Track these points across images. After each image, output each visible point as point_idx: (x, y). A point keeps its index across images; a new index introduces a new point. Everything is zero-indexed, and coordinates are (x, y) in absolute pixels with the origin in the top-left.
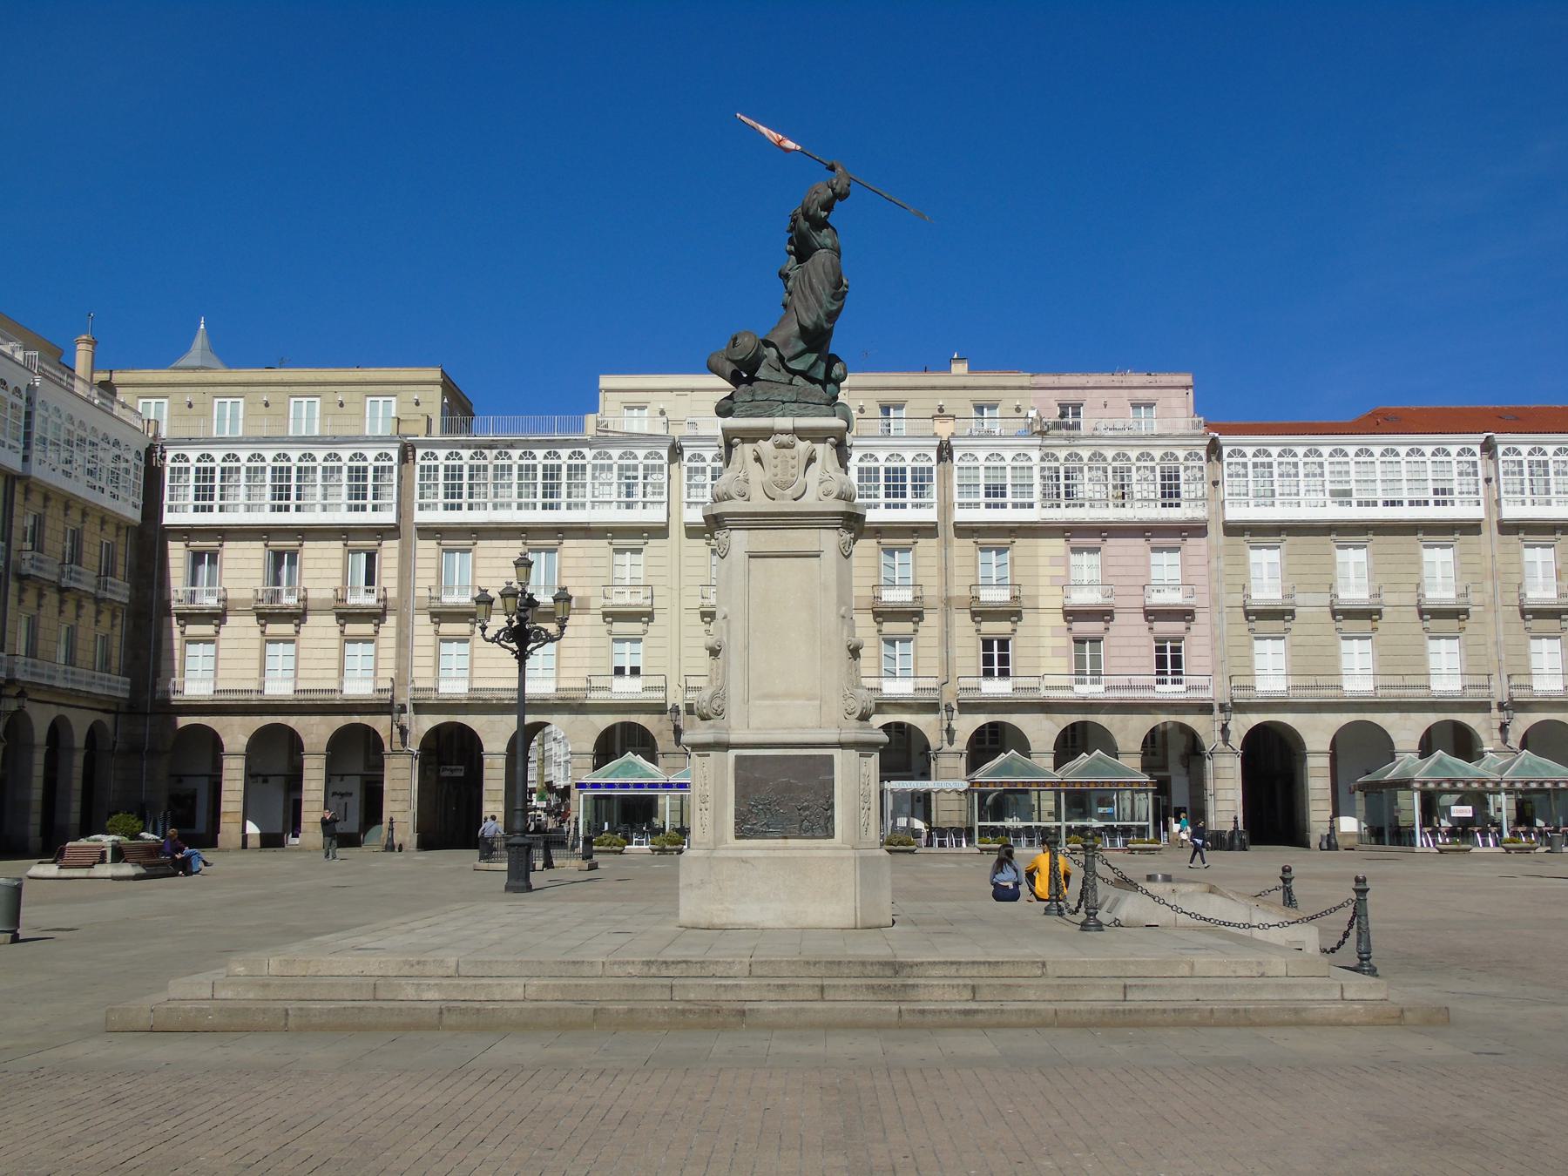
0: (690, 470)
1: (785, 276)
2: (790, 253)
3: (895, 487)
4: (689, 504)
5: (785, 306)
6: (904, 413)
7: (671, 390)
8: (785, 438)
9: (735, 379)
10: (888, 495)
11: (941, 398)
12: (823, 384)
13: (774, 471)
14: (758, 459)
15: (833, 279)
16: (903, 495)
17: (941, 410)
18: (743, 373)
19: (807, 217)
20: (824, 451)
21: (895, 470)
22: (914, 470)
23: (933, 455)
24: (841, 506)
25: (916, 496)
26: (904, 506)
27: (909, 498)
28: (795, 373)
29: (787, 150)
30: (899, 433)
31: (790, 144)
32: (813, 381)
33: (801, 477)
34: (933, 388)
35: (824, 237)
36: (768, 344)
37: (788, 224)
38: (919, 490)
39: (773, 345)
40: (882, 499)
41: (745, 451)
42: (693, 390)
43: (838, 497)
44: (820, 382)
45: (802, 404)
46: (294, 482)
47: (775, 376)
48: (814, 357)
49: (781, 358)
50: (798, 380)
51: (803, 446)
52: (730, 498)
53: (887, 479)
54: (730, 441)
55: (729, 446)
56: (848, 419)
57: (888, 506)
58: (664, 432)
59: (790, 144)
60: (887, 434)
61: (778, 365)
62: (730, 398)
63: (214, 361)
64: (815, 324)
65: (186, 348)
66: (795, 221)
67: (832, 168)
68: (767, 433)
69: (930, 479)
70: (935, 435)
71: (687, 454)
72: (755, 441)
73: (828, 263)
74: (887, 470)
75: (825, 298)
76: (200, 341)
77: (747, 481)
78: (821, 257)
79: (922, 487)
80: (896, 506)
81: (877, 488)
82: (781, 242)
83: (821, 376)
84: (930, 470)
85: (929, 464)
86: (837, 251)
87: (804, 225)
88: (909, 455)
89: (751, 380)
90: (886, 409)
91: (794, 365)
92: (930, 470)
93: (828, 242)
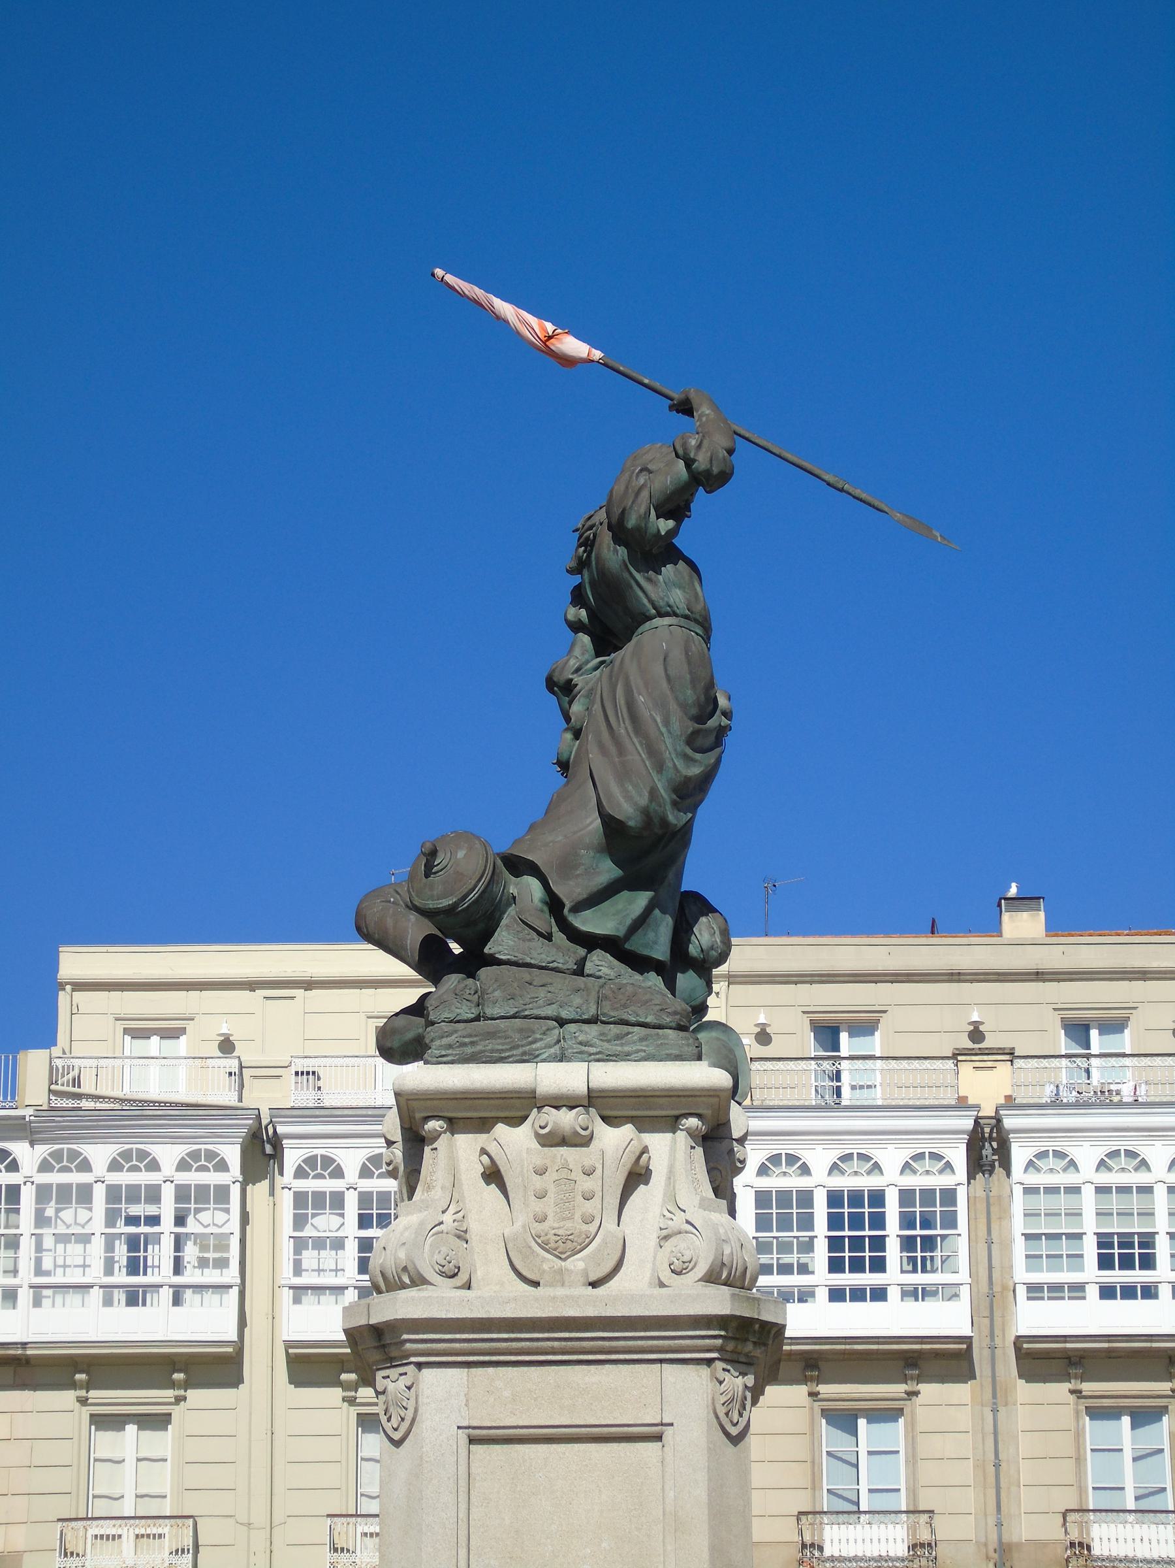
0: (300, 1199)
1: (563, 689)
2: (576, 627)
3: (857, 1243)
4: (299, 1292)
5: (564, 766)
6: (875, 1044)
7: (251, 985)
8: (566, 1119)
9: (431, 961)
10: (835, 1266)
11: (978, 1004)
12: (667, 971)
13: (537, 1206)
14: (493, 1176)
15: (690, 695)
16: (879, 1265)
17: (976, 1034)
18: (453, 944)
19: (619, 531)
20: (672, 1152)
21: (856, 1198)
22: (906, 1196)
23: (958, 1155)
24: (719, 1302)
25: (913, 1265)
26: (879, 1294)
27: (894, 1275)
28: (590, 942)
29: (568, 361)
30: (863, 1097)
31: (573, 346)
32: (639, 963)
33: (610, 1224)
34: (955, 977)
35: (667, 586)
36: (517, 865)
37: (568, 551)
38: (921, 1249)
39: (534, 870)
40: (821, 1276)
41: (456, 1155)
42: (309, 985)
43: (711, 1278)
44: (658, 967)
45: (614, 1029)
47: (539, 952)
48: (642, 899)
49: (554, 904)
50: (601, 963)
51: (615, 1141)
52: (419, 1281)
53: (834, 1222)
54: (417, 1128)
55: (415, 1141)
56: (732, 1062)
57: (836, 1295)
58: (230, 1098)
59: (573, 346)
60: (833, 1101)
61: (546, 922)
62: (418, 1009)
64: (646, 812)
66: (588, 543)
67: (685, 408)
68: (516, 1107)
69: (950, 1221)
70: (962, 1104)
71: (293, 1157)
72: (483, 1125)
73: (677, 655)
74: (834, 1199)
75: (671, 745)
77: (462, 1236)
78: (658, 639)
79: (929, 1243)
80: (858, 1295)
81: (808, 1246)
82: (553, 599)
83: (661, 951)
84: (949, 1196)
85: (946, 1181)
86: (703, 624)
87: (613, 555)
88: (891, 1157)
89: (475, 961)
90: (828, 1033)
91: (590, 922)
92: (949, 1196)
93: (677, 598)
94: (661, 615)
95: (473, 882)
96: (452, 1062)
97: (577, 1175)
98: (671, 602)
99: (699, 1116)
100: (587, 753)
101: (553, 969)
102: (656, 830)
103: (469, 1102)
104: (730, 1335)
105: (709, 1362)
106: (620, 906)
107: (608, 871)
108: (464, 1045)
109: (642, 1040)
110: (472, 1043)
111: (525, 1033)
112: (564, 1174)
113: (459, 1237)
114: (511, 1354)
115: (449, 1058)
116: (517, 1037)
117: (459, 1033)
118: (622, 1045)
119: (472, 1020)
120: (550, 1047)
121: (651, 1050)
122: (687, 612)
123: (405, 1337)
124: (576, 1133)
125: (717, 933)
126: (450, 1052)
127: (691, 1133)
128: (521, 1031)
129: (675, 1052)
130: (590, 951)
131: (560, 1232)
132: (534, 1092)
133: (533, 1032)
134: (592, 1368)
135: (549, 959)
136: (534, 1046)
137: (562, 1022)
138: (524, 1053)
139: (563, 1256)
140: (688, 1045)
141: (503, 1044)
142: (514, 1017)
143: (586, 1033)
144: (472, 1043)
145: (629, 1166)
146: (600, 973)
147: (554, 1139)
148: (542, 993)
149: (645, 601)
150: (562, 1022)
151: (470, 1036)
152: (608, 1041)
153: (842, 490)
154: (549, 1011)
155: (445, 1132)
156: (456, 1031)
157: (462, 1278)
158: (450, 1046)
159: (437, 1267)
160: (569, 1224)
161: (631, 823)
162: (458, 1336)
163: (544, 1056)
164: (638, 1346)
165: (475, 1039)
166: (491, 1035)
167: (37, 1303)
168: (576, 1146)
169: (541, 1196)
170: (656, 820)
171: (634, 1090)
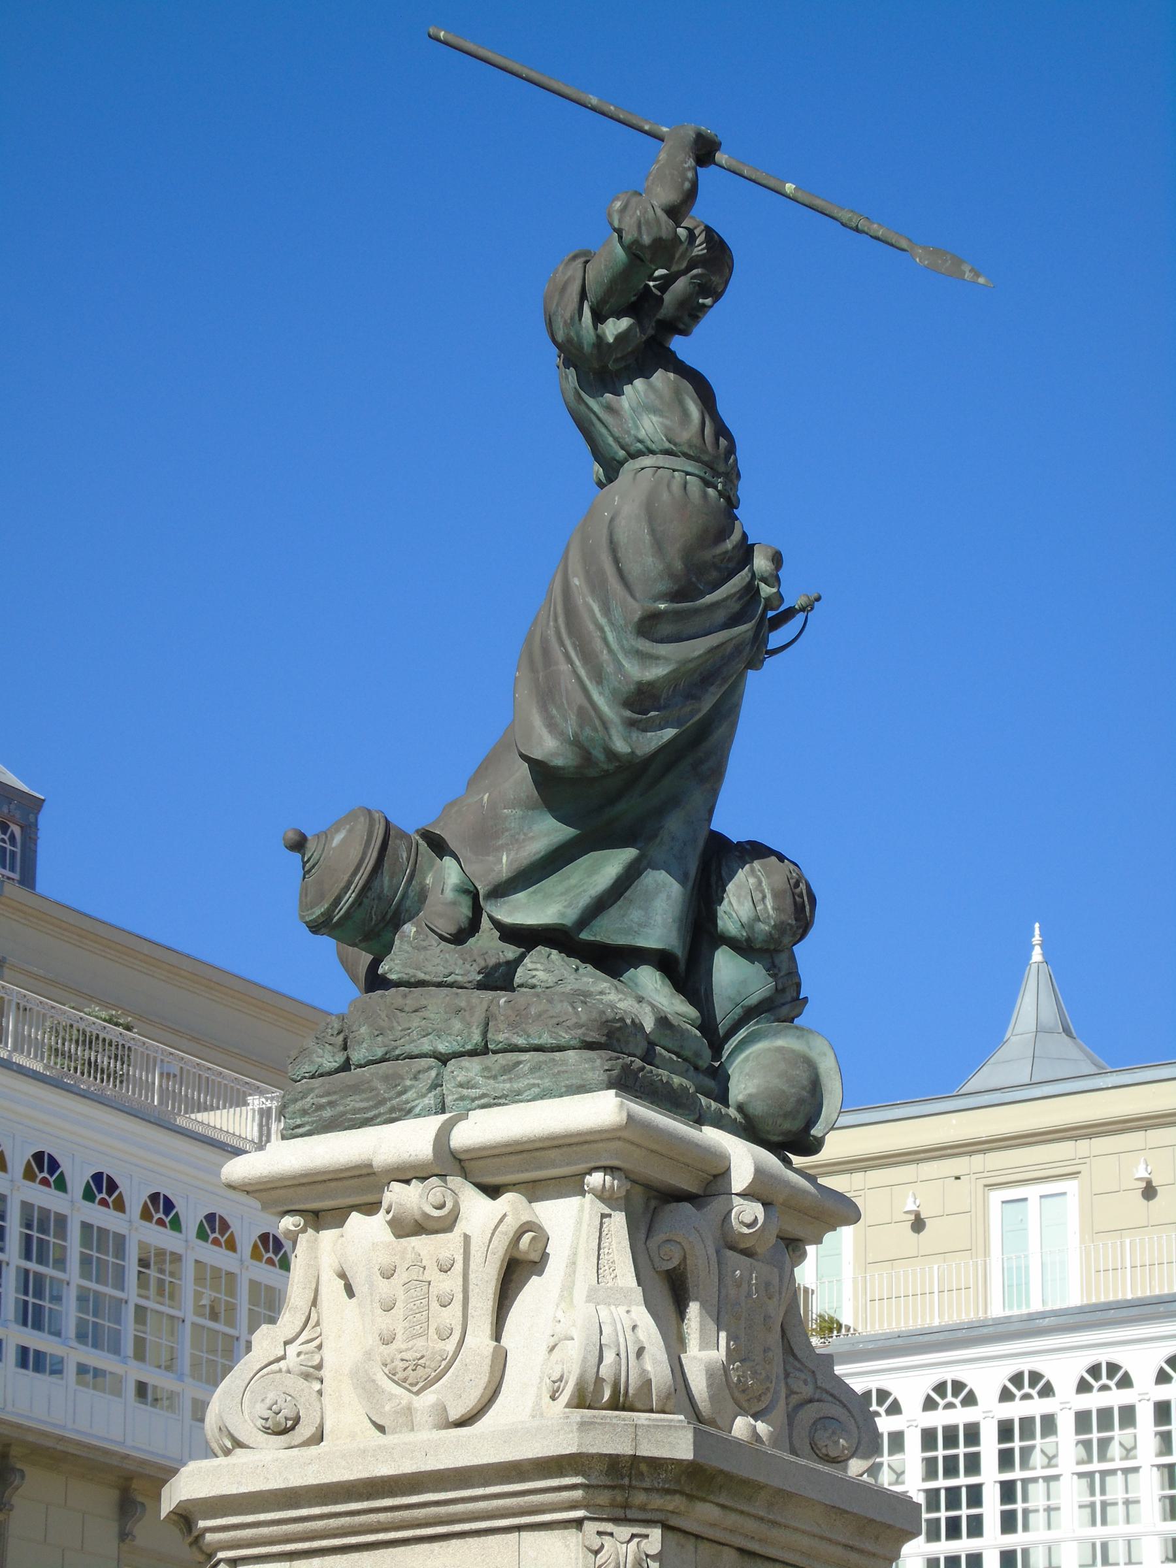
8: (405, 1197)
13: (384, 1322)
28: (525, 938)
46: (990, 1476)
48: (610, 865)
50: (542, 967)
51: (483, 1217)
63: (1070, 1055)
65: (990, 1034)
68: (357, 1190)
76: (1033, 1004)
77: (313, 1373)
94: (633, 456)
95: (346, 878)
96: (309, 1134)
97: (432, 1274)
98: (642, 434)
99: (605, 1169)
100: (657, 665)
101: (451, 985)
102: (605, 767)
103: (321, 1187)
104: (594, 1482)
105: (578, 1523)
106: (573, 881)
107: (548, 832)
108: (320, 1107)
109: (533, 1070)
110: (331, 1104)
111: (392, 1080)
112: (415, 1273)
113: (307, 1376)
114: (335, 1536)
115: (307, 1128)
116: (381, 1087)
117: (316, 1091)
118: (510, 1080)
119: (338, 1070)
120: (424, 1096)
121: (547, 1083)
122: (667, 445)
123: (202, 1524)
124: (426, 1216)
125: (769, 896)
126: (306, 1119)
127: (602, 1195)
128: (386, 1078)
129: (576, 1082)
130: (529, 949)
131: (405, 1355)
132: (370, 1166)
133: (403, 1079)
134: (471, 1541)
135: (446, 972)
136: (404, 1097)
137: (443, 1059)
138: (392, 1110)
139: (415, 1389)
140: (593, 1069)
141: (367, 1100)
142: (383, 1060)
143: (468, 1070)
144: (331, 1104)
145: (501, 1252)
146: (534, 981)
147: (409, 1227)
148: (416, 1022)
149: (610, 440)
150: (443, 1059)
151: (328, 1094)
152: (495, 1077)
153: (857, 230)
154: (426, 1046)
155: (304, 1231)
156: (312, 1090)
157: (305, 1430)
158: (304, 1112)
159: (260, 1422)
160: (420, 1343)
161: (559, 762)
162: (262, 1517)
163: (417, 1110)
164: (498, 1509)
165: (333, 1098)
166: (355, 1089)
167: (1081, 1475)
168: (437, 1232)
169: (388, 1308)
170: (598, 754)
171: (507, 1145)
